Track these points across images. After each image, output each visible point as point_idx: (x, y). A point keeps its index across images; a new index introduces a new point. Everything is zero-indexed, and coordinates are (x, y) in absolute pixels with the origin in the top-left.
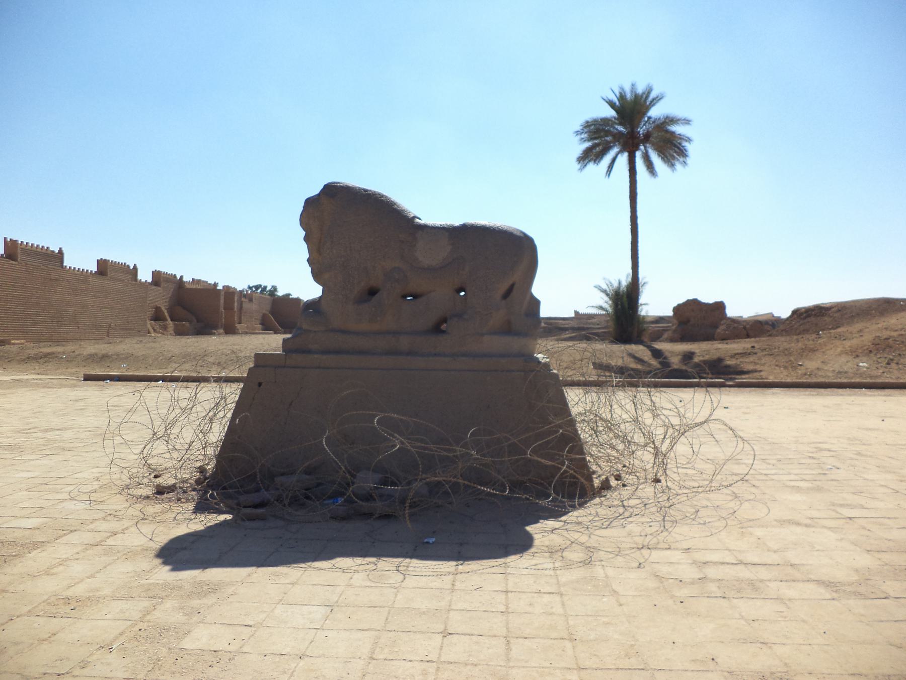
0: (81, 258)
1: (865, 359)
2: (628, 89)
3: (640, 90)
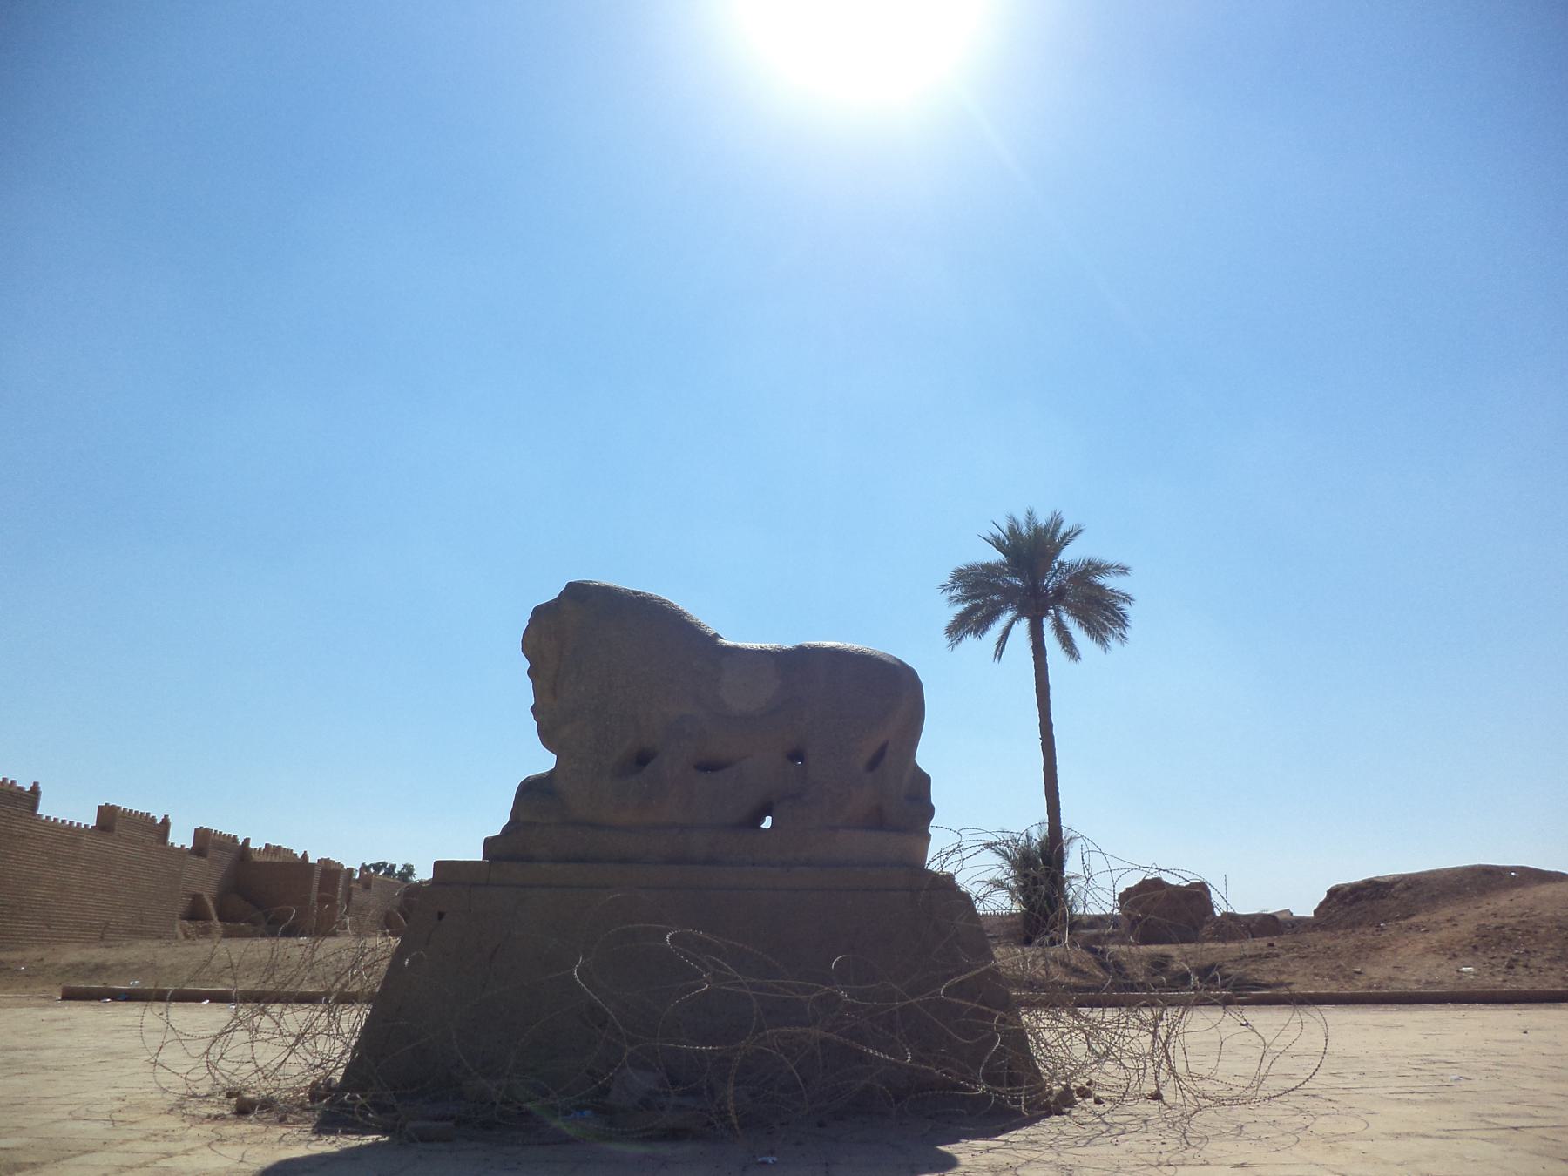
0: (69, 804)
1: (1468, 960)
2: (1021, 519)
3: (1042, 520)
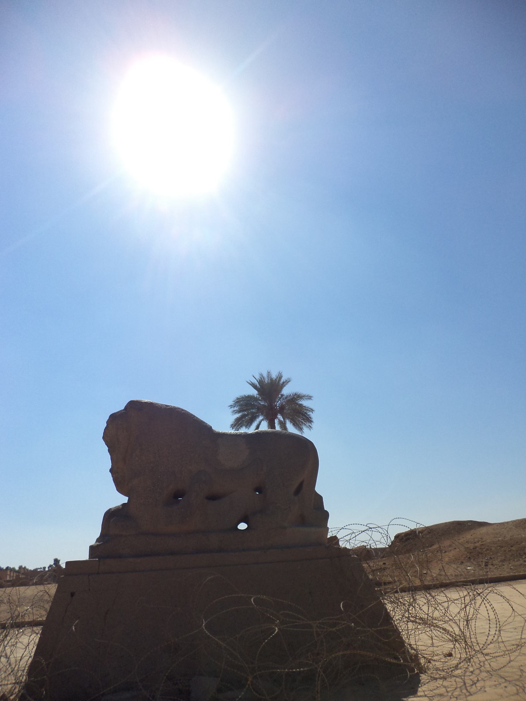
2: (265, 375)
3: (274, 376)
